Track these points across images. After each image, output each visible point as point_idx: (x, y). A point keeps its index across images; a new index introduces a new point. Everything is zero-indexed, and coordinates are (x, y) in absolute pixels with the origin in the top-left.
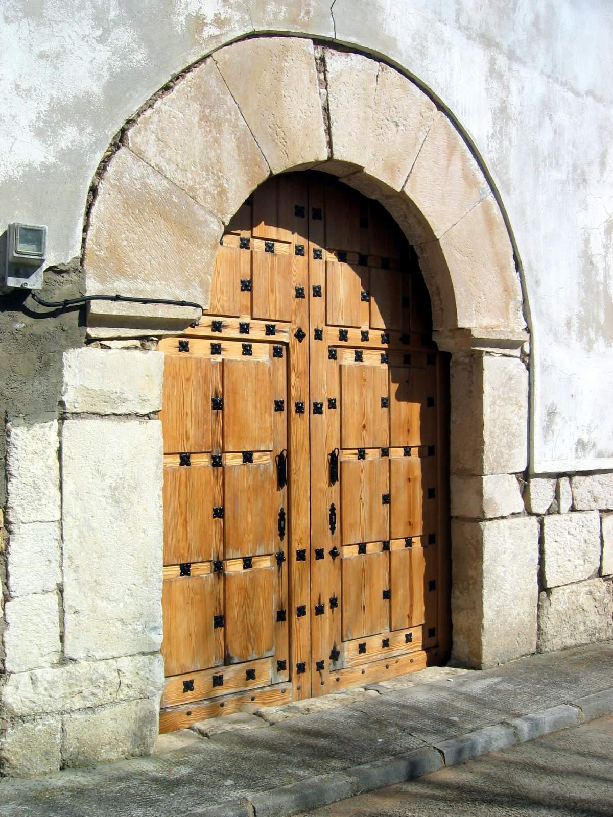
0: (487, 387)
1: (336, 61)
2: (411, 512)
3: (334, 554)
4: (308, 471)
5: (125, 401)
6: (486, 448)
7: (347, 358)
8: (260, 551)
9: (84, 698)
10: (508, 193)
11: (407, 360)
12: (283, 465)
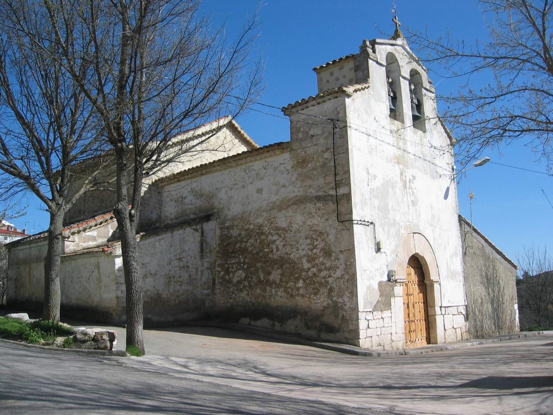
1: (415, 235)
4: (411, 306)
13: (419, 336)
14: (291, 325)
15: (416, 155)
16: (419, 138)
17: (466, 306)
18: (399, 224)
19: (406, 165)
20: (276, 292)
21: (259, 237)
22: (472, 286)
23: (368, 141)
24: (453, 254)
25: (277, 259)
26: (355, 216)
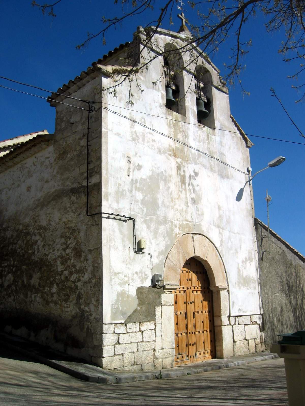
0: (221, 298)
1: (195, 236)
2: (207, 324)
3: (195, 333)
4: (190, 316)
5: (169, 302)
6: (222, 310)
7: (195, 292)
8: (183, 332)
9: (165, 356)
10: (223, 257)
11: (205, 293)
12: (186, 314)
13: (201, 350)
14: (45, 336)
15: (201, 150)
16: (205, 134)
17: (262, 315)
18: (172, 222)
19: (186, 159)
20: (35, 297)
21: (26, 238)
22: (270, 293)
23: (132, 127)
24: (246, 258)
25: (37, 261)
26: (106, 207)
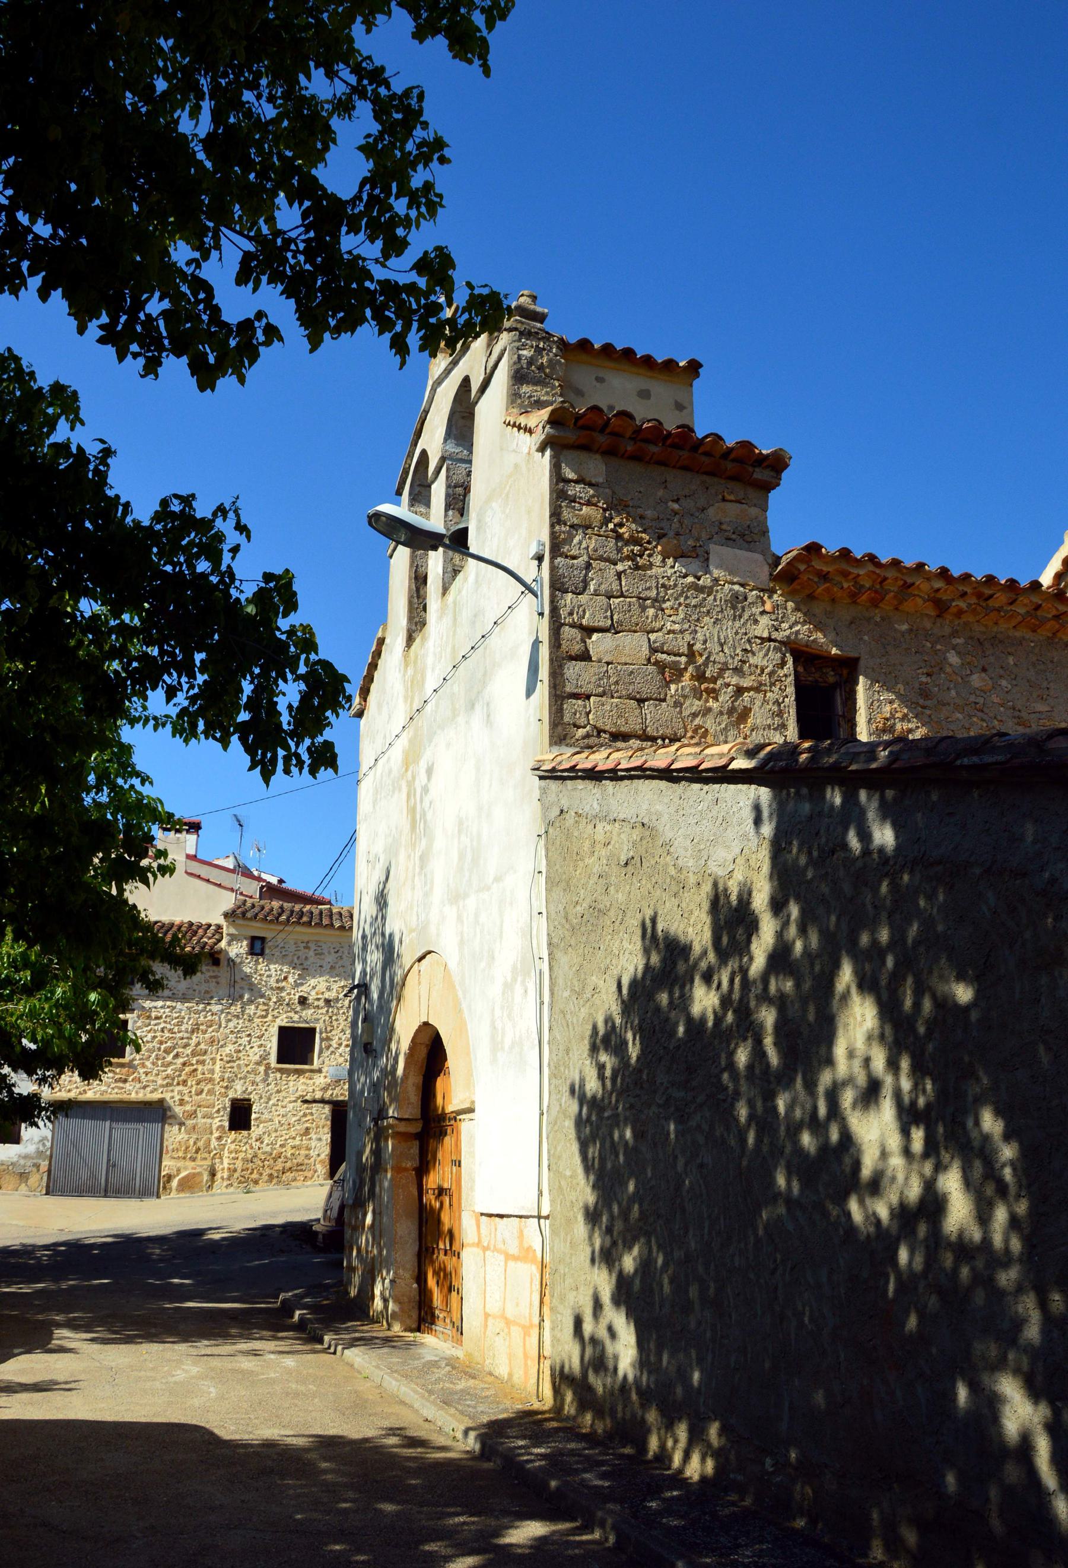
24: (514, 969)
